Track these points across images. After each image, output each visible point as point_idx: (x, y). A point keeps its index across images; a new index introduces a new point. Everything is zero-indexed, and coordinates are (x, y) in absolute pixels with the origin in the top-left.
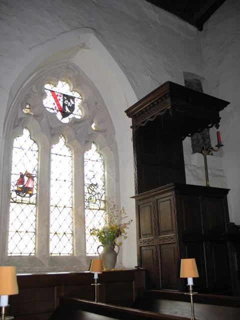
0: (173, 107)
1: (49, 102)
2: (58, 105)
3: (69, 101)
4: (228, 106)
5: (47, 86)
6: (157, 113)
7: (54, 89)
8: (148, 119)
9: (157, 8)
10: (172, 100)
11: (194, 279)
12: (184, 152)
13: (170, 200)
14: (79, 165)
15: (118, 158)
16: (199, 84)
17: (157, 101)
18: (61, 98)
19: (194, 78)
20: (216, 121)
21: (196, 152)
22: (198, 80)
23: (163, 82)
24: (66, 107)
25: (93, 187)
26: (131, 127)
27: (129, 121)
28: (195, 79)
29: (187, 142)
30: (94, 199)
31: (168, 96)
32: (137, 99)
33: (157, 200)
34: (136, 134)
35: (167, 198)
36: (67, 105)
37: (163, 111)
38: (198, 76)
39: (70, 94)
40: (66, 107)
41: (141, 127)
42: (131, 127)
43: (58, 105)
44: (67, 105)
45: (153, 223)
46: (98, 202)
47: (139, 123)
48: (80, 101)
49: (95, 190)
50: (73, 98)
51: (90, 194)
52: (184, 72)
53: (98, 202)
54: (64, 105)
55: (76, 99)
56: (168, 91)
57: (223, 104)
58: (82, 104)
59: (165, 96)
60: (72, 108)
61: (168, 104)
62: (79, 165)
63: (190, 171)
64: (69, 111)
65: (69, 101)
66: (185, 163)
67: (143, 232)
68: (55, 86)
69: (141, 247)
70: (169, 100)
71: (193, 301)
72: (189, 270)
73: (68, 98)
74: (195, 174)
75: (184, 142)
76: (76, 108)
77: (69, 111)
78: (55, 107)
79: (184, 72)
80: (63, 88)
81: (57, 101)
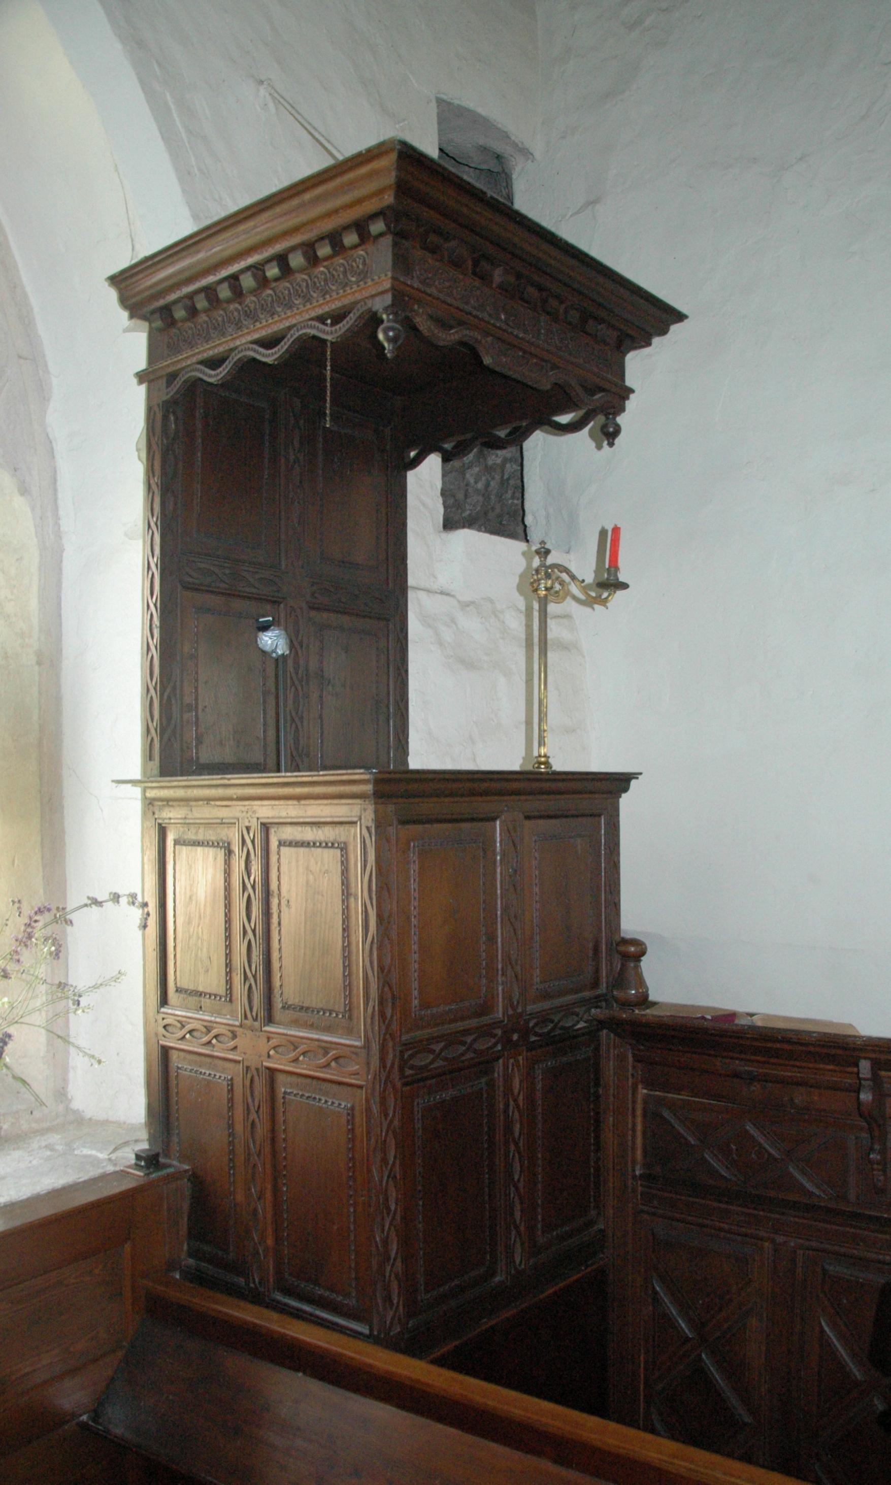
0: (401, 299)
4: (674, 328)
6: (299, 317)
8: (242, 342)
9: (145, 431)
10: (402, 262)
13: (343, 848)
15: (59, 535)
16: (500, 173)
17: (309, 249)
19: (482, 141)
20: (600, 404)
21: (470, 523)
22: (498, 157)
23: (351, 145)
26: (141, 377)
27: (133, 345)
28: (484, 149)
29: (426, 480)
31: (377, 227)
32: (185, 212)
33: (266, 827)
34: (165, 417)
35: (325, 834)
37: (338, 317)
38: (505, 136)
41: (194, 385)
42: (141, 377)
45: (239, 948)
47: (187, 360)
52: (440, 101)
56: (389, 199)
57: (649, 317)
59: (360, 226)
61: (369, 283)
63: (426, 620)
66: (411, 581)
67: (180, 972)
69: (165, 1052)
70: (381, 255)
74: (448, 636)
75: (413, 477)
79: (440, 101)
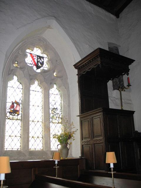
0: (101, 63)
1: (29, 60)
2: (34, 62)
3: (41, 59)
4: (134, 62)
5: (28, 51)
6: (92, 66)
7: (32, 52)
8: (87, 70)
10: (101, 59)
11: (114, 164)
12: (108, 89)
13: (100, 117)
14: (47, 97)
15: (69, 93)
16: (117, 49)
17: (92, 59)
18: (36, 58)
19: (114, 46)
20: (127, 71)
22: (116, 47)
23: (96, 48)
24: (39, 63)
25: (54, 110)
26: (77, 75)
27: (76, 71)
28: (114, 47)
29: (110, 83)
30: (55, 117)
31: (98, 56)
32: (80, 58)
33: (92, 117)
34: (80, 78)
35: (98, 117)
36: (39, 62)
37: (96, 65)
38: (117, 45)
39: (41, 55)
40: (39, 63)
41: (83, 75)
42: (77, 75)
43: (34, 62)
44: (39, 62)
45: (90, 131)
46: (57, 119)
47: (82, 72)
48: (47, 59)
49: (56, 111)
50: (43, 58)
51: (53, 114)
52: (108, 42)
53: (57, 119)
54: (38, 62)
55: (44, 58)
56: (99, 54)
57: (131, 61)
58: (48, 61)
59: (97, 56)
60: (42, 64)
61: (99, 61)
62: (47, 97)
63: (112, 100)
64: (41, 65)
65: (41, 59)
66: (109, 96)
67: (84, 136)
68: (32, 50)
69: (83, 145)
70: (99, 59)
71: (113, 177)
72: (111, 158)
73: (40, 57)
74: (114, 102)
75: (108, 83)
76: (45, 63)
77: (41, 65)
78: (33, 63)
79: (108, 42)
80: (37, 52)
81: (33, 59)
